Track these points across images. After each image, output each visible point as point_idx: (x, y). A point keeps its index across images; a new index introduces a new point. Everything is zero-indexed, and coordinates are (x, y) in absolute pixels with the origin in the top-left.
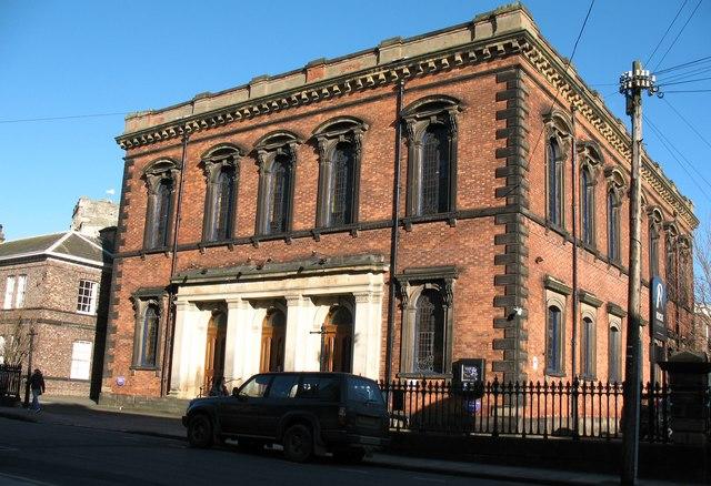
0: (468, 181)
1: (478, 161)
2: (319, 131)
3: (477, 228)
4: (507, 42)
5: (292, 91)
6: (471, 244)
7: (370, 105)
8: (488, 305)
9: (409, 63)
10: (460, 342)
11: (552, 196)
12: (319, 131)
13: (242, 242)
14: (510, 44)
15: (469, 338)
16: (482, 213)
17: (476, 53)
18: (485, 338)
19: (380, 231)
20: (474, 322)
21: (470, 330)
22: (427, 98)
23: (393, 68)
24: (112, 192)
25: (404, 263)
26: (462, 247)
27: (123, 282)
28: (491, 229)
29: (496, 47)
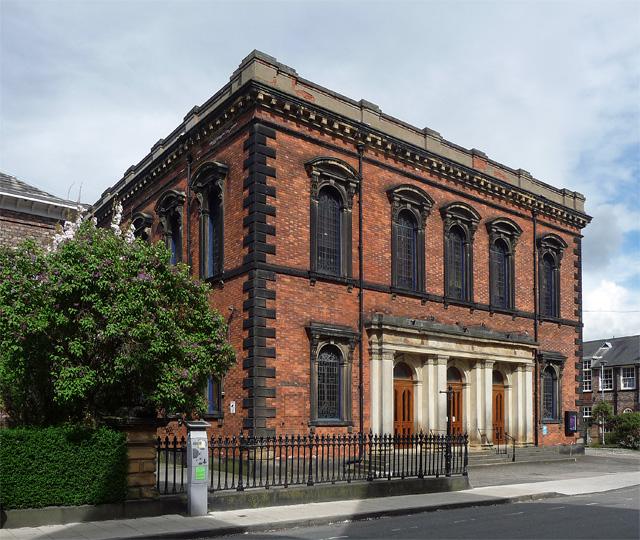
27: (278, 307)
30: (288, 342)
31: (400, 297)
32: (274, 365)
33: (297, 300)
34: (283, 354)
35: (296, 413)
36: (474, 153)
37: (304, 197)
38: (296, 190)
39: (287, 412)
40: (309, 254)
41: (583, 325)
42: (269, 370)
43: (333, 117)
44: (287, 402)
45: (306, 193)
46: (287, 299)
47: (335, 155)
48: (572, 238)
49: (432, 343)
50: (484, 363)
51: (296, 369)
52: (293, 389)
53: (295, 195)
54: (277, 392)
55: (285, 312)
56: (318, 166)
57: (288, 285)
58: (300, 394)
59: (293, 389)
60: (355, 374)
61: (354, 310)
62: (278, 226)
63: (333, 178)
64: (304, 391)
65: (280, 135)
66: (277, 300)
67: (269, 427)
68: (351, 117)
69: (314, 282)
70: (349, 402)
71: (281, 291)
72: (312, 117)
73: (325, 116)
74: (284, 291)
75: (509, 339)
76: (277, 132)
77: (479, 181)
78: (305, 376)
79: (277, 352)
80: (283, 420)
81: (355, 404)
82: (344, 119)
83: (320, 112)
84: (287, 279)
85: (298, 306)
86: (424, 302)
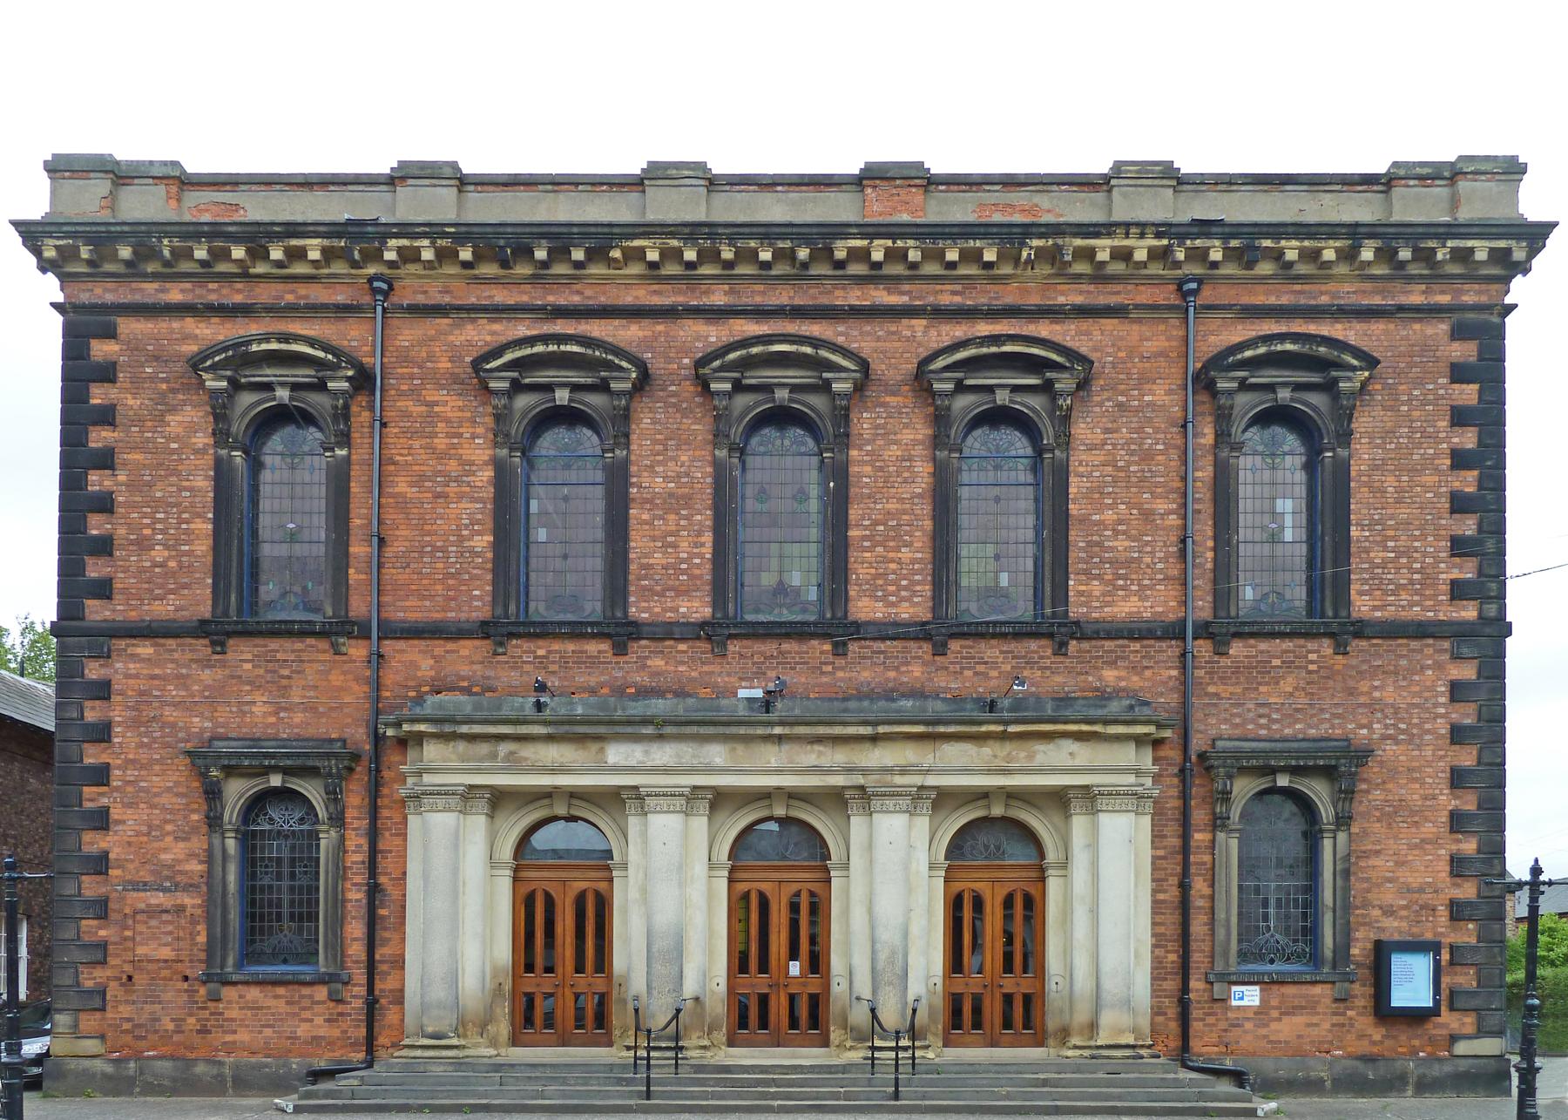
0: (1378, 556)
1: (1403, 513)
2: (940, 363)
3: (1403, 662)
4: (1502, 244)
5: (840, 230)
6: (1389, 694)
7: (1086, 324)
8: (1436, 825)
9: (1234, 236)
10: (1366, 904)
11: (215, 184)
12: (940, 363)
13: (667, 632)
14: (1508, 252)
15: (1389, 896)
16: (1421, 631)
17: (1416, 250)
18: (1426, 897)
19: (1136, 646)
20: (1399, 864)
21: (1390, 880)
22: (1282, 337)
23: (1182, 237)
24: (358, 522)
25: (1211, 728)
26: (1362, 700)
27: (117, 715)
28: (1438, 666)
29: (1471, 250)
30: (146, 790)
31: (526, 645)
32: (103, 845)
33: (173, 692)
34: (128, 821)
35: (166, 953)
36: (873, 176)
37: (196, 452)
38: (177, 439)
39: (140, 950)
40: (210, 581)
41: (1507, 630)
42: (89, 858)
43: (823, 235)
44: (140, 928)
45: (202, 439)
46: (142, 693)
47: (254, 328)
48: (1443, 328)
49: (616, 754)
50: (640, 798)
51: (165, 850)
52: (158, 899)
53: (174, 451)
54: (111, 905)
55: (135, 724)
56: (214, 367)
57: (148, 660)
58: (180, 909)
59: (158, 899)
60: (356, 857)
61: (356, 695)
62: (122, 531)
63: (1285, 384)
64: (190, 901)
65: (129, 327)
66: (115, 698)
67: (89, 984)
68: (420, 219)
69: (223, 644)
70: (337, 921)
71: (128, 676)
72: (727, 254)
73: (236, 239)
74: (137, 676)
75: (773, 716)
76: (119, 320)
77: (863, 255)
78: (196, 867)
79: (115, 814)
80: (128, 968)
81: (355, 929)
82: (294, 229)
83: (783, 237)
84: (145, 649)
85: (175, 705)
86: (840, 650)
